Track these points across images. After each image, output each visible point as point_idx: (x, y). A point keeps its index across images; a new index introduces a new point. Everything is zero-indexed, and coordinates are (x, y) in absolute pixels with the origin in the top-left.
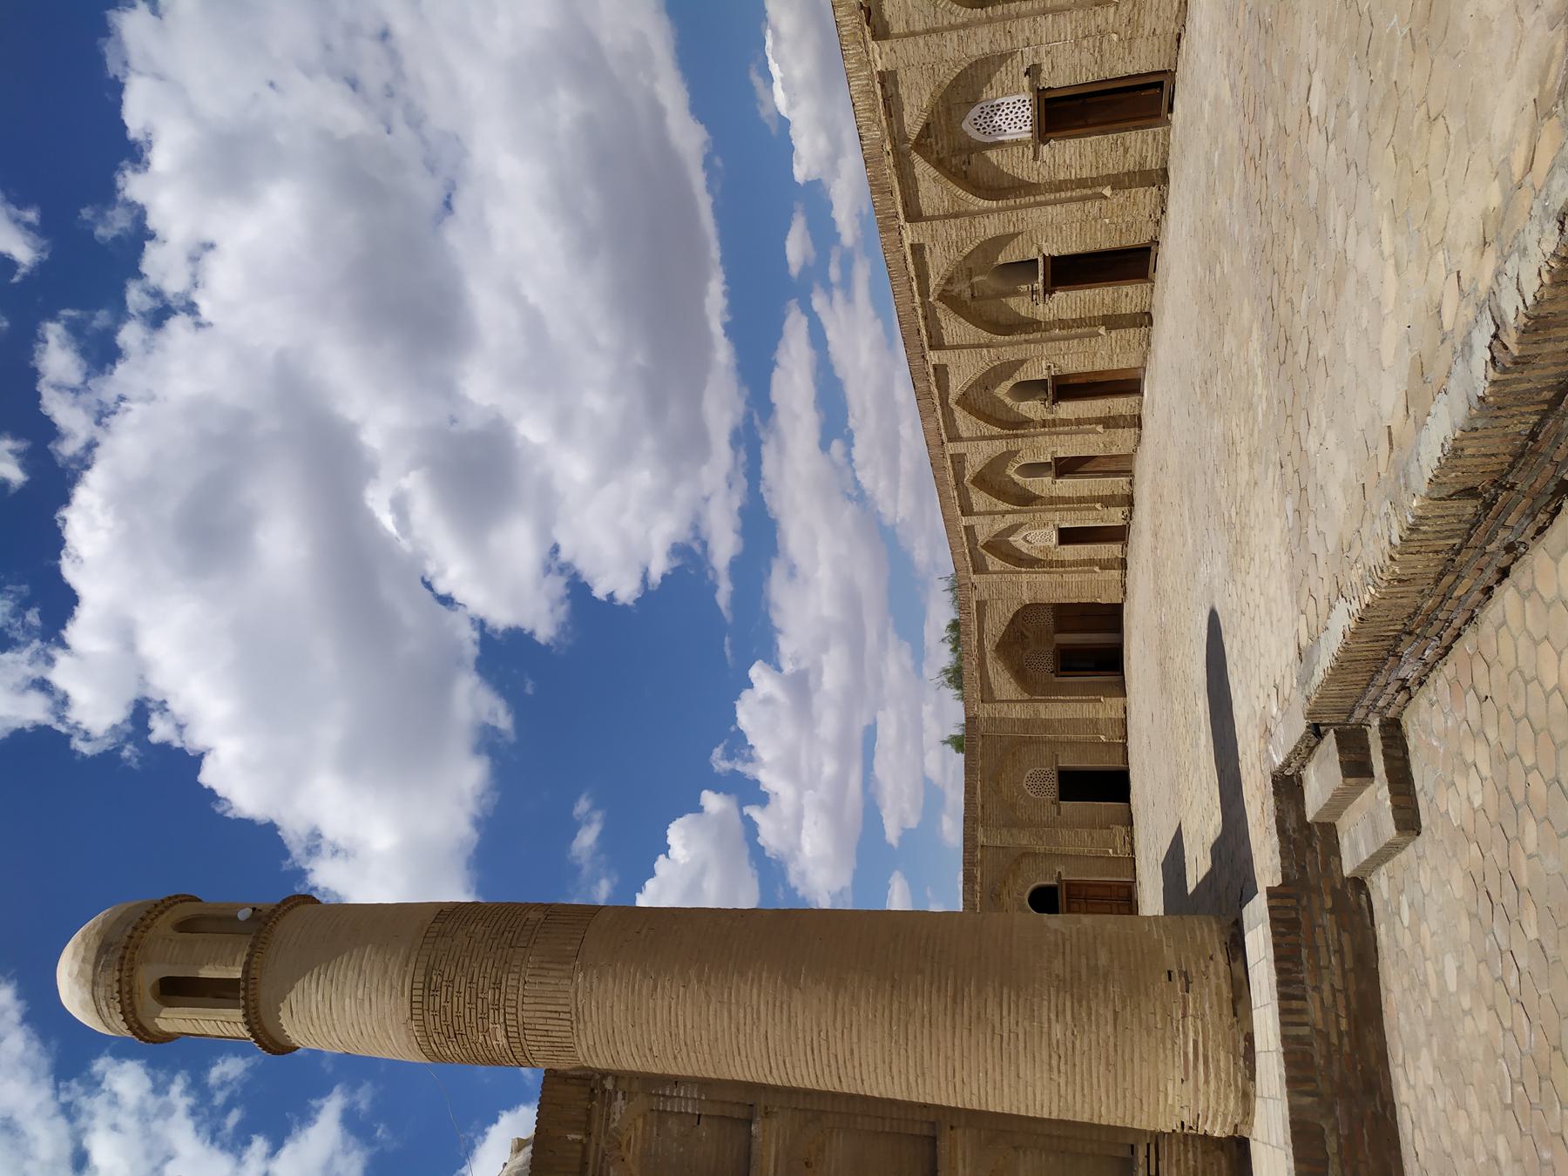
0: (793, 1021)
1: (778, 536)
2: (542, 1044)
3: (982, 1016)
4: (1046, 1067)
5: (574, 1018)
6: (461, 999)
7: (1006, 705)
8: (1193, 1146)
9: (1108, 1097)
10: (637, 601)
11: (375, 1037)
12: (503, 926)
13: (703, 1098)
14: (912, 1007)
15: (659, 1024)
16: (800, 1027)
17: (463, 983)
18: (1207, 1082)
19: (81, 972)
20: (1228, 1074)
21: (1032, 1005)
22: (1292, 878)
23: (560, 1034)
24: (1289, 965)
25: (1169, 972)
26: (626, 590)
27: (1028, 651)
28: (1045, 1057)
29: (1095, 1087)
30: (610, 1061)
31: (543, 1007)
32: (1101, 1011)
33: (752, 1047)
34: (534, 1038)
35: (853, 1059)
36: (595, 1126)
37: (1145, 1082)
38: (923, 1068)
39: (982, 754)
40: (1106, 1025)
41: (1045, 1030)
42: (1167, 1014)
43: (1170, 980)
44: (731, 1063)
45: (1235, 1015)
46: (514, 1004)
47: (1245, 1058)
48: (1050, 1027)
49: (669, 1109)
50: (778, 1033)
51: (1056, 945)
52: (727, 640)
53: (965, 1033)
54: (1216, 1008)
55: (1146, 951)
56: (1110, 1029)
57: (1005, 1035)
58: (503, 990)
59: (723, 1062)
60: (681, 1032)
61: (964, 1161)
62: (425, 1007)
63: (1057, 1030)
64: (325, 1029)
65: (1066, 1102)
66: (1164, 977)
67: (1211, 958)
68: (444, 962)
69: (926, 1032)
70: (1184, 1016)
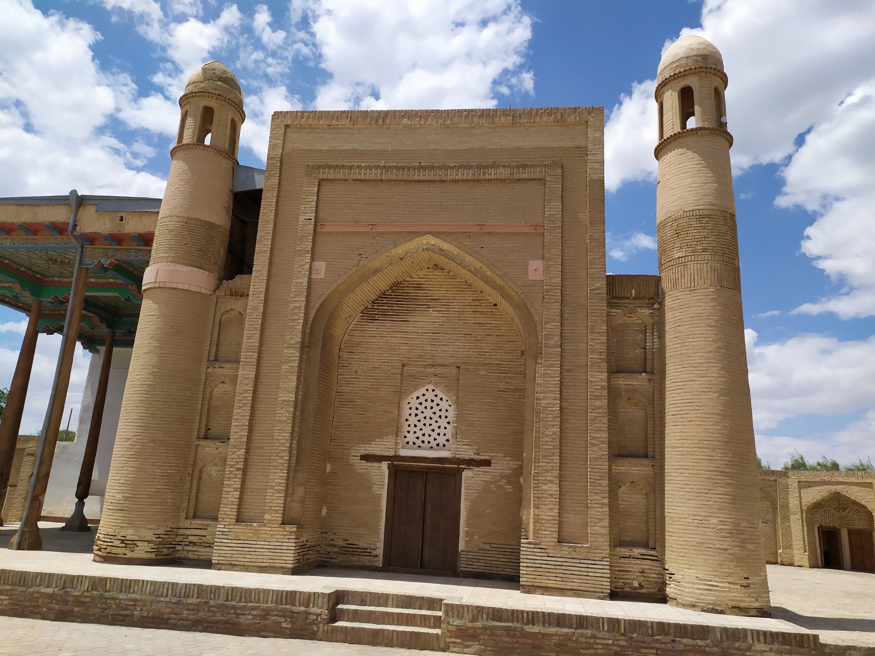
0: (702, 394)
1: (855, 342)
2: (677, 274)
3: (716, 485)
4: (695, 513)
5: (692, 288)
6: (696, 234)
7: (798, 495)
8: (659, 578)
9: (683, 541)
10: (804, 254)
11: (672, 196)
12: (731, 248)
13: (654, 350)
14: (717, 451)
15: (693, 329)
16: (700, 397)
17: (704, 234)
18: (698, 589)
19: (692, 49)
20: (704, 600)
21: (725, 509)
22: (825, 648)
23: (683, 282)
24: (780, 639)
25: (748, 578)
26: (811, 247)
27: (834, 511)
28: (700, 514)
29: (688, 536)
30: (670, 307)
31: (696, 273)
32: (726, 543)
33: (687, 374)
34: (679, 270)
35: (687, 421)
36: (637, 302)
37: (694, 560)
38: (687, 455)
39: (764, 480)
40: (720, 545)
41: (713, 515)
42: (729, 575)
43: (745, 578)
44: (676, 364)
45: (733, 607)
46: (696, 259)
47: (712, 609)
48: (715, 517)
49: (647, 334)
50: (696, 386)
51: (753, 524)
52: (776, 313)
53: (708, 476)
54: (735, 598)
55: (756, 568)
56: (718, 546)
57: (708, 495)
58: (702, 253)
59: (677, 360)
60: (691, 340)
61: (640, 470)
62: (690, 218)
63: (714, 521)
64: (673, 172)
65: (677, 521)
66: (746, 576)
67: (757, 600)
68: (713, 223)
69: (705, 457)
70: (729, 583)
